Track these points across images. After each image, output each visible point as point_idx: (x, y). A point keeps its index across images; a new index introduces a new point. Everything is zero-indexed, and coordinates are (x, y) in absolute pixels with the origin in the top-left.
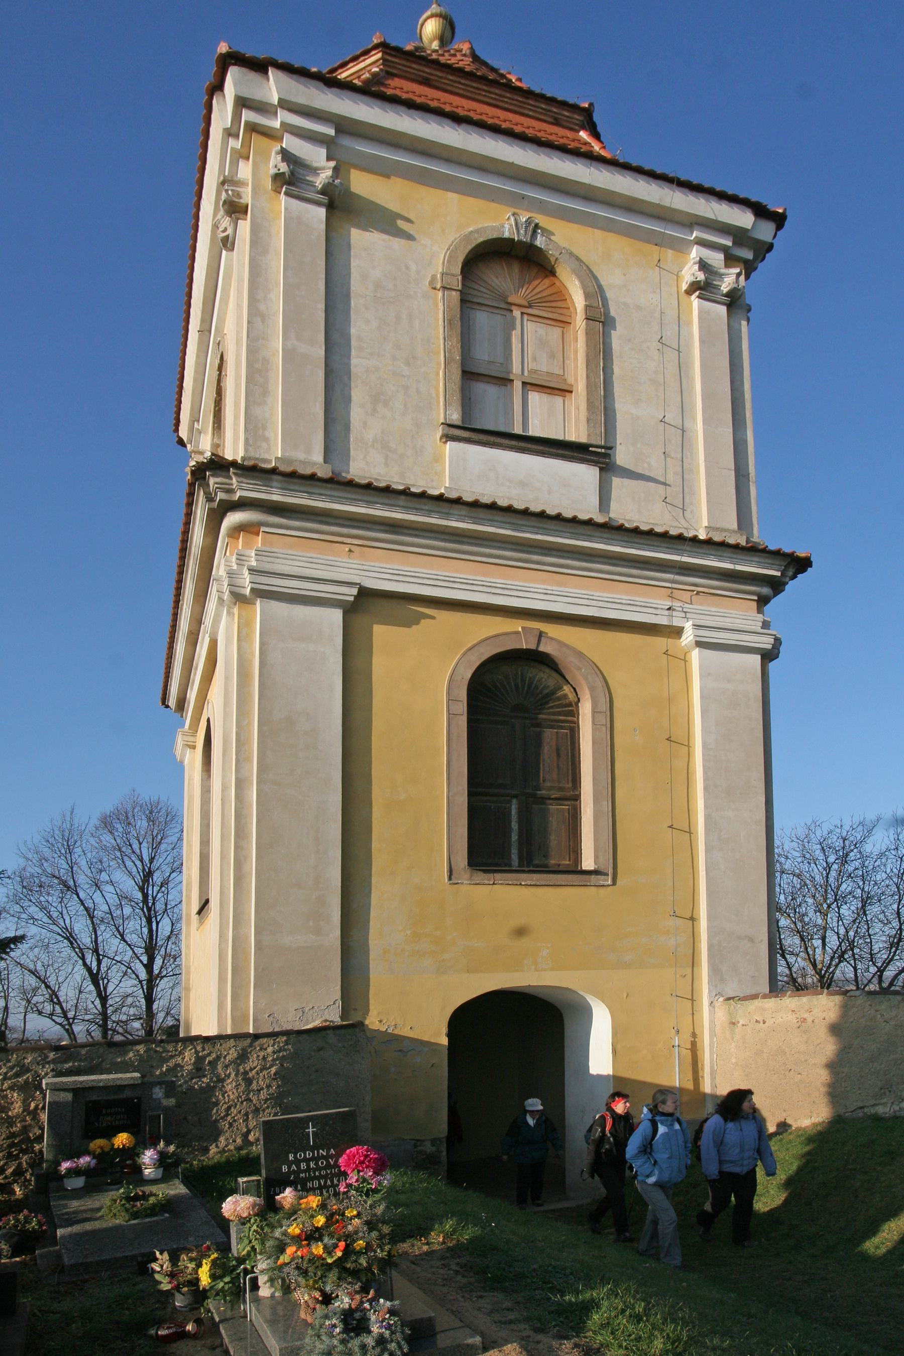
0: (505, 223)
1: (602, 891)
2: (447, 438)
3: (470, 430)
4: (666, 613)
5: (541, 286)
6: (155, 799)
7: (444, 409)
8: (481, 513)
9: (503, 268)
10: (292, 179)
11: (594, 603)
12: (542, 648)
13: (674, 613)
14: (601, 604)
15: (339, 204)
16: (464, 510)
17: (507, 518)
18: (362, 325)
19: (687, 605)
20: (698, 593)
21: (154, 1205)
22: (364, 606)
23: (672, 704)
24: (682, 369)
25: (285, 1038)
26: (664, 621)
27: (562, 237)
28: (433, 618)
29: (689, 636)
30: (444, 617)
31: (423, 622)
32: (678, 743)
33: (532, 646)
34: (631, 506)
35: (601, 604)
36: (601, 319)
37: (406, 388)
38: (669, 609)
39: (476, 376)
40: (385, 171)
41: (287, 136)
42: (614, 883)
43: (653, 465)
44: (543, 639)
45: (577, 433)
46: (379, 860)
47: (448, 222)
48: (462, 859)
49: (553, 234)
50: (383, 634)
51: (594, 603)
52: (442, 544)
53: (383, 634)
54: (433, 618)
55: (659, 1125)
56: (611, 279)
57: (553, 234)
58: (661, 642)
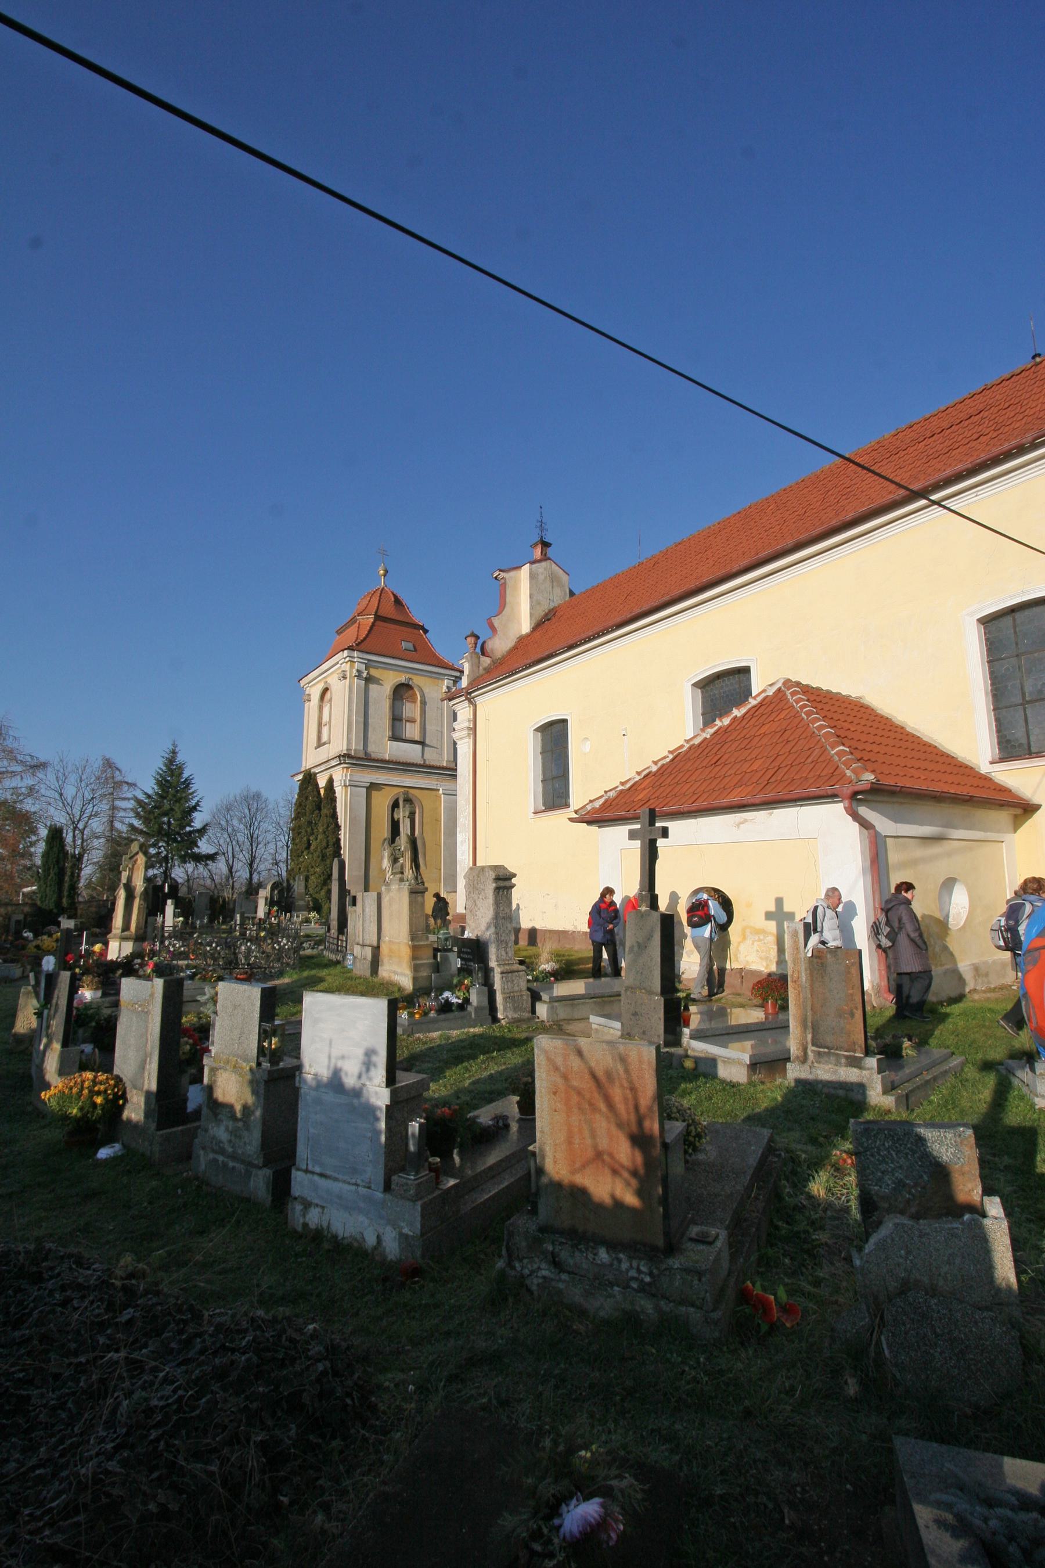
0: (402, 678)
3: (395, 737)
5: (410, 692)
6: (254, 789)
7: (388, 733)
9: (402, 691)
10: (359, 674)
15: (369, 680)
18: (371, 711)
21: (44, 871)
22: (373, 787)
23: (436, 810)
24: (442, 715)
27: (417, 681)
29: (441, 792)
30: (387, 788)
32: (438, 821)
34: (431, 757)
36: (424, 703)
39: (396, 719)
43: (434, 743)
45: (417, 738)
47: (390, 679)
50: (374, 793)
53: (374, 793)
55: (929, 1134)
56: (426, 691)
58: (434, 792)
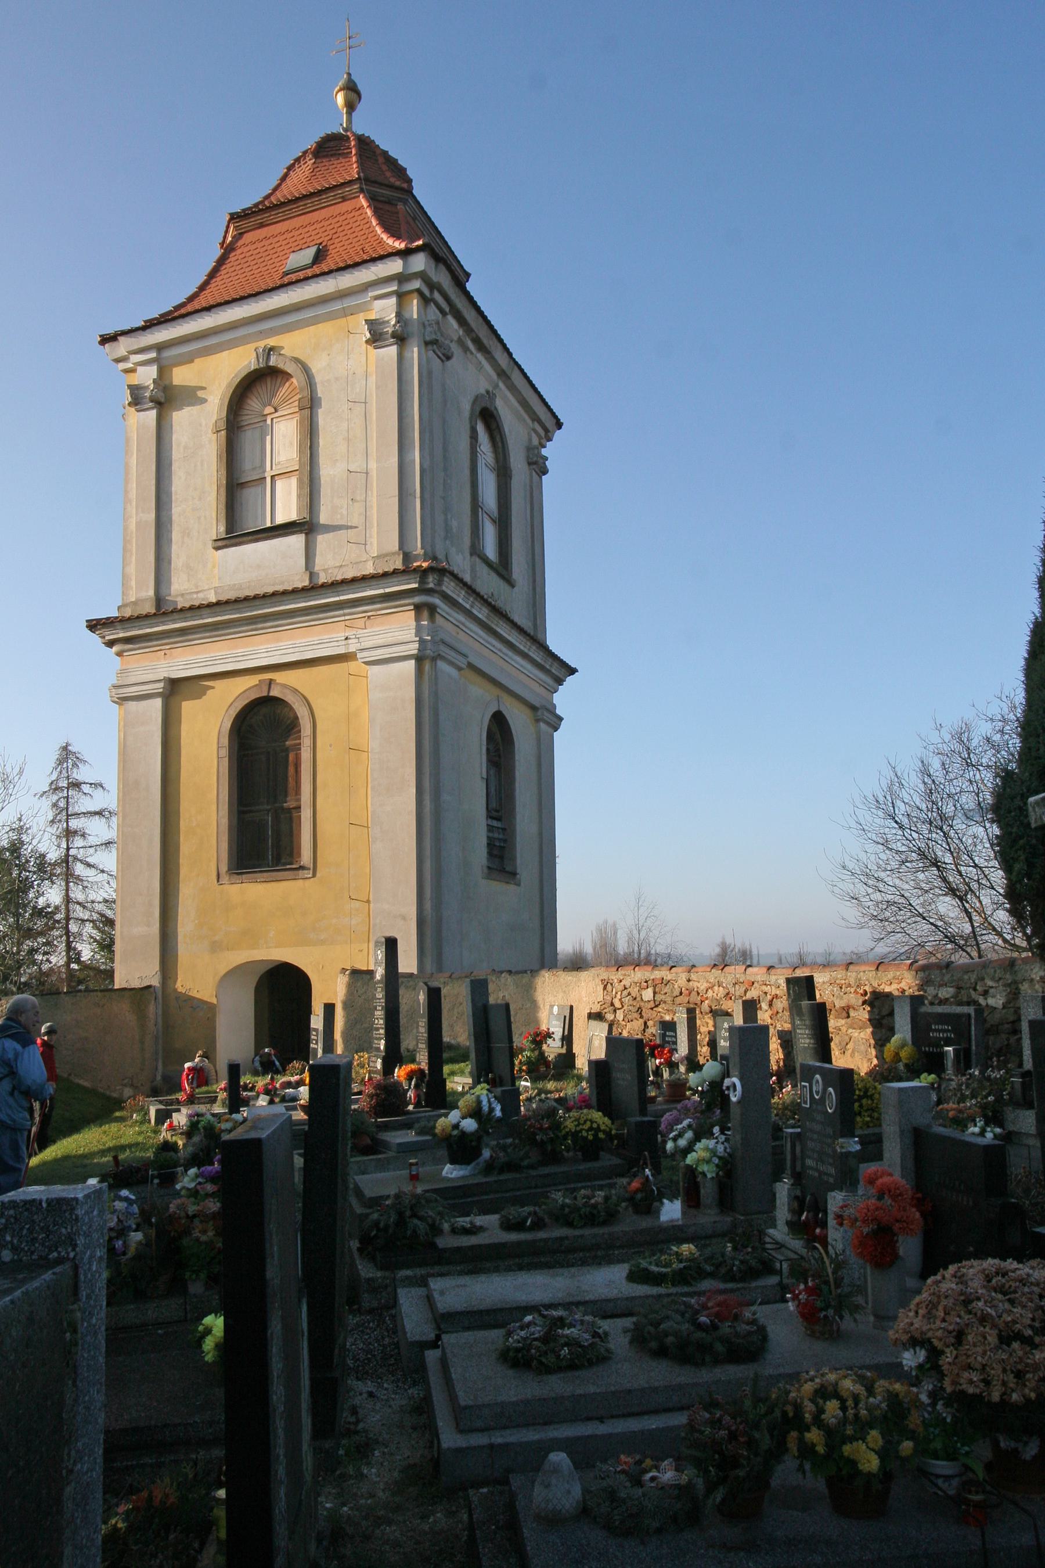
1: (307, 882)
2: (217, 548)
4: (344, 643)
8: (217, 609)
11: (297, 650)
12: (271, 694)
13: (350, 641)
14: (302, 649)
16: (208, 610)
17: (228, 607)
19: (361, 631)
20: (369, 617)
22: (176, 689)
25: (71, 884)
26: (342, 651)
27: (293, 344)
28: (213, 688)
30: (219, 684)
31: (209, 692)
33: (265, 694)
35: (302, 649)
37: (199, 518)
38: (346, 639)
40: (189, 359)
41: (139, 368)
42: (314, 875)
44: (273, 686)
46: (184, 871)
48: (224, 868)
49: (283, 348)
51: (297, 650)
52: (208, 634)
54: (213, 688)
57: (283, 348)
